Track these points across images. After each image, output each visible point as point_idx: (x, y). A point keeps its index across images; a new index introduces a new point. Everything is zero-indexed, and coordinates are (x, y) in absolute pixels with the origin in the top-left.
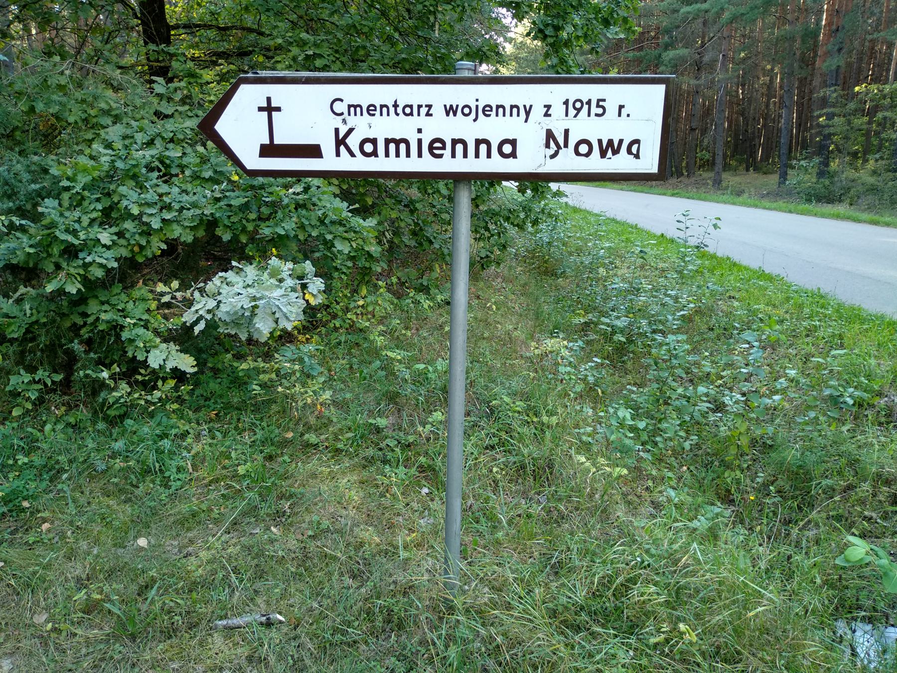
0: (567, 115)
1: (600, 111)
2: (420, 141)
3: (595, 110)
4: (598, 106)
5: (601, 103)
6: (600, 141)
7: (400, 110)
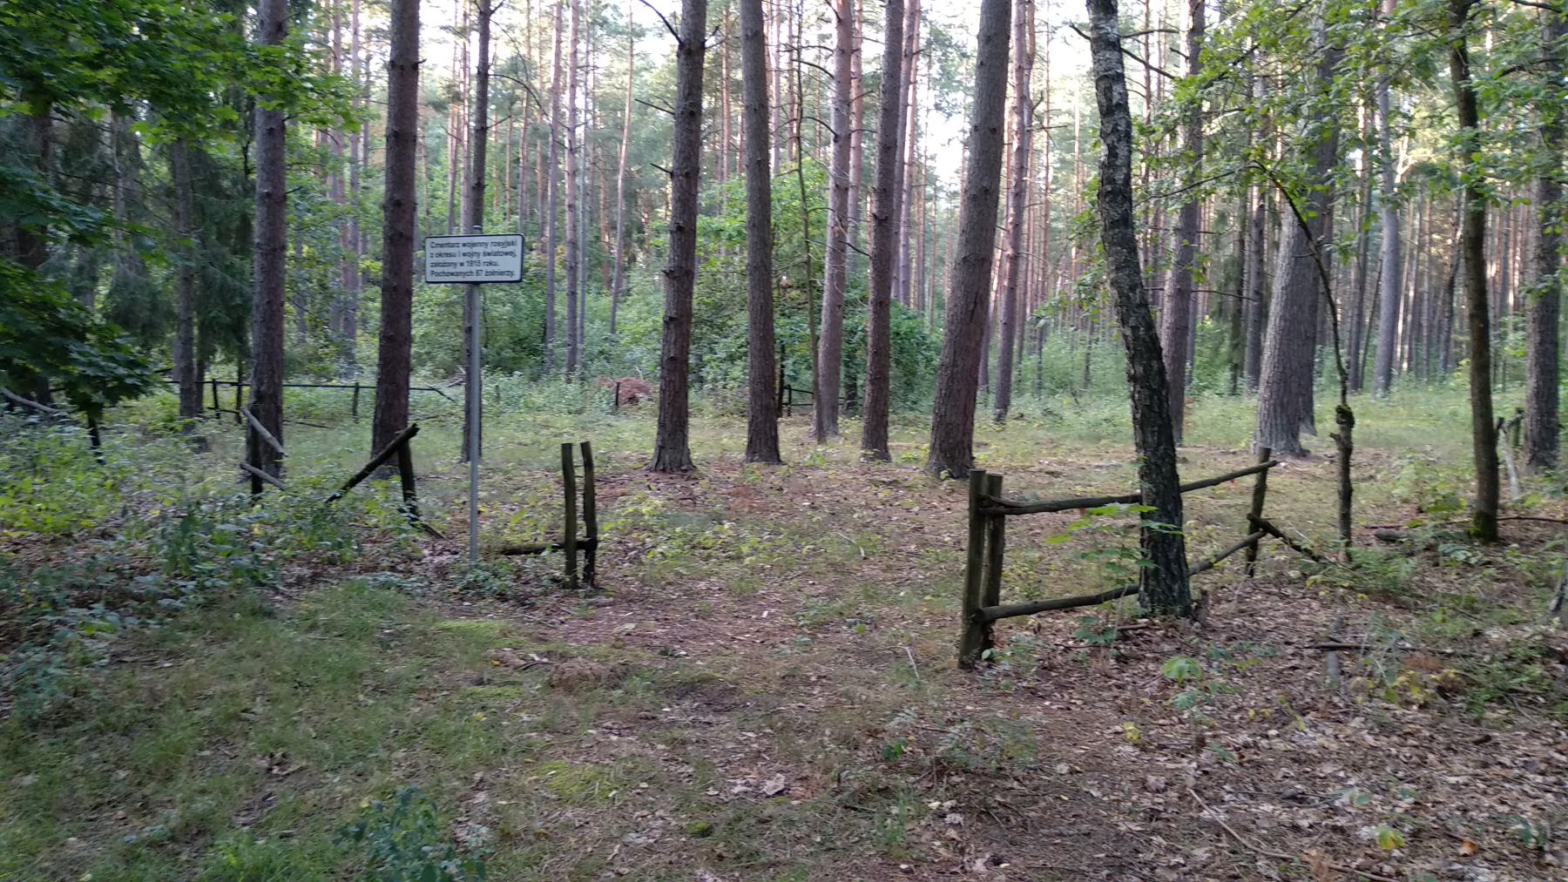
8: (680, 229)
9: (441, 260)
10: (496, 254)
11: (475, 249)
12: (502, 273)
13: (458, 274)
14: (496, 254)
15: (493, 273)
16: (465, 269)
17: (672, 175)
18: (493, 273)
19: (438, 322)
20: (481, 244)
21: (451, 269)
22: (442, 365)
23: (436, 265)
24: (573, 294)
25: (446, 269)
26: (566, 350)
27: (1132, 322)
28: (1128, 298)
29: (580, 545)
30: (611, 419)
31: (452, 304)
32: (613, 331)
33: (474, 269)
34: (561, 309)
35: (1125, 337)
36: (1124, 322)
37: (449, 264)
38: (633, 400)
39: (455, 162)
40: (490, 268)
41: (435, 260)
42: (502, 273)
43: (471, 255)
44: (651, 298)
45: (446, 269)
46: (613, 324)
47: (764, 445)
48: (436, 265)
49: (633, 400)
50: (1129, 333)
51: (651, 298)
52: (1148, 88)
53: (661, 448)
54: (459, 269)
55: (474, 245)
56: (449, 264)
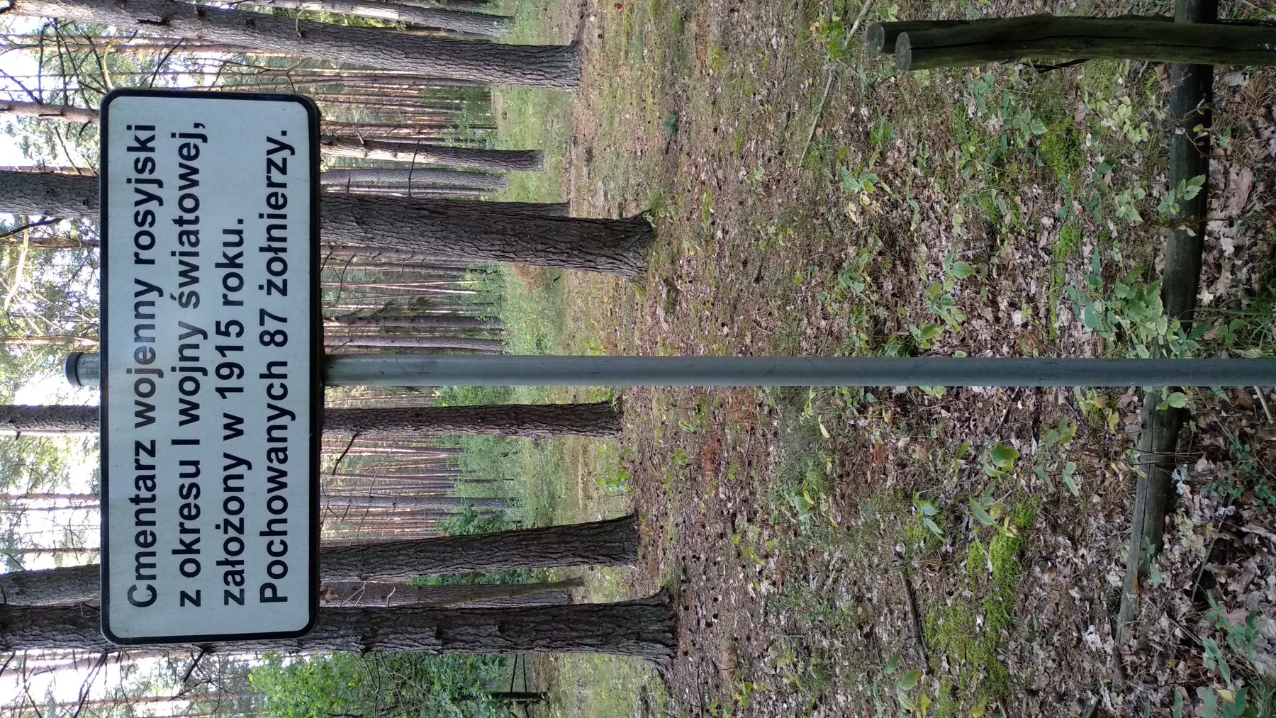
0: (240, 390)
1: (234, 329)
2: (270, 216)
3: (231, 341)
4: (227, 334)
5: (223, 329)
6: (181, 188)
7: (187, 216)
9: (211, 547)
12: (277, 203)
13: (278, 452)
15: (275, 250)
16: (252, 404)
18: (275, 250)
21: (255, 484)
23: (233, 572)
25: (256, 516)
33: (254, 357)
40: (254, 266)
41: (211, 581)
42: (277, 203)
43: (190, 372)
45: (256, 516)
48: (233, 572)
52: (1067, 65)
54: (253, 445)
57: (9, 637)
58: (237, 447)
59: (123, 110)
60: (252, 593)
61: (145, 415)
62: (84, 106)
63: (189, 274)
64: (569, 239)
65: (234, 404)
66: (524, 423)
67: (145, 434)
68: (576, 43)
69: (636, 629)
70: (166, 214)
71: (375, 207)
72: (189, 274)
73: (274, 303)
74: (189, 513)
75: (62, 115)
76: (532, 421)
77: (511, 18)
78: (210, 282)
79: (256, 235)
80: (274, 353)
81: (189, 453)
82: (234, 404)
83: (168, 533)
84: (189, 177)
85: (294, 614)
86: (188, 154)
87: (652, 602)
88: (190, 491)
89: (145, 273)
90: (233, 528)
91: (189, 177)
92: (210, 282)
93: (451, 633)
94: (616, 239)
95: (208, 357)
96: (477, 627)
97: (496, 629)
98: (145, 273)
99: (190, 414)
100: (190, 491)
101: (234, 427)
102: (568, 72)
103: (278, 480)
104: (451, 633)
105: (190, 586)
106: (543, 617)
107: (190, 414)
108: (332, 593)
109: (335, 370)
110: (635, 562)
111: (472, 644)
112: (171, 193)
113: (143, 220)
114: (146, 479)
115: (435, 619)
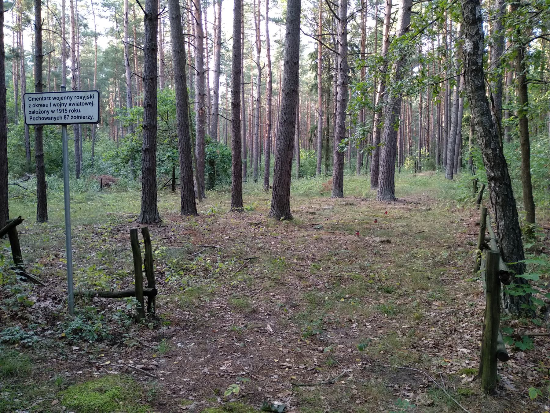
8: (149, 105)
9: (37, 109)
10: (79, 104)
11: (63, 101)
12: (84, 117)
13: (50, 118)
14: (79, 104)
15: (77, 117)
16: (56, 114)
17: (144, 79)
18: (77, 117)
19: (13, 154)
20: (67, 98)
21: (45, 115)
22: (17, 172)
23: (34, 112)
24: (77, 141)
25: (41, 115)
26: (75, 164)
27: (492, 146)
28: (490, 132)
29: (145, 293)
30: (100, 194)
31: (19, 146)
32: (93, 156)
33: (62, 115)
34: (72, 148)
35: (487, 155)
36: (487, 145)
37: (44, 112)
38: (108, 185)
39: (17, 86)
40: (75, 114)
41: (32, 109)
42: (84, 117)
43: (60, 105)
44: (108, 142)
45: (41, 115)
46: (93, 152)
47: (189, 206)
48: (34, 112)
49: (108, 185)
50: (490, 152)
51: (108, 142)
53: (144, 212)
54: (51, 115)
55: (62, 98)
56: (44, 112)
57: (147, 21)
58: (50, 112)
59: (96, 94)
60: (31, 115)
61: (54, 99)
62: (392, 12)
63: (73, 104)
64: (280, 191)
65: (56, 112)
66: (235, 178)
67: (51, 99)
68: (395, 200)
69: (147, 211)
70: (81, 101)
71: (290, 126)
72: (73, 104)
73: (70, 117)
74: (41, 105)
75: (388, 4)
76: (235, 181)
77: (452, 178)
78: (72, 108)
79: (79, 114)
80: (63, 117)
81: (49, 105)
82: (56, 112)
83: (38, 102)
84: (87, 104)
85: (28, 122)
86: (90, 104)
87: (156, 216)
88: (44, 105)
89: (73, 98)
90: (39, 112)
91: (87, 104)
92: (72, 108)
93: (147, 153)
94: (282, 207)
95: (62, 108)
96: (149, 161)
97: (148, 166)
98: (73, 98)
99: (54, 105)
100: (44, 105)
101: (53, 112)
102: (383, 197)
103: (46, 119)
104: (147, 153)
105: (31, 106)
106: (151, 181)
107: (54, 105)
108: (202, 113)
109: (64, 127)
110: (181, 214)
111: (144, 160)
112: (85, 101)
113: (81, 97)
114: (46, 99)
115: (152, 148)
